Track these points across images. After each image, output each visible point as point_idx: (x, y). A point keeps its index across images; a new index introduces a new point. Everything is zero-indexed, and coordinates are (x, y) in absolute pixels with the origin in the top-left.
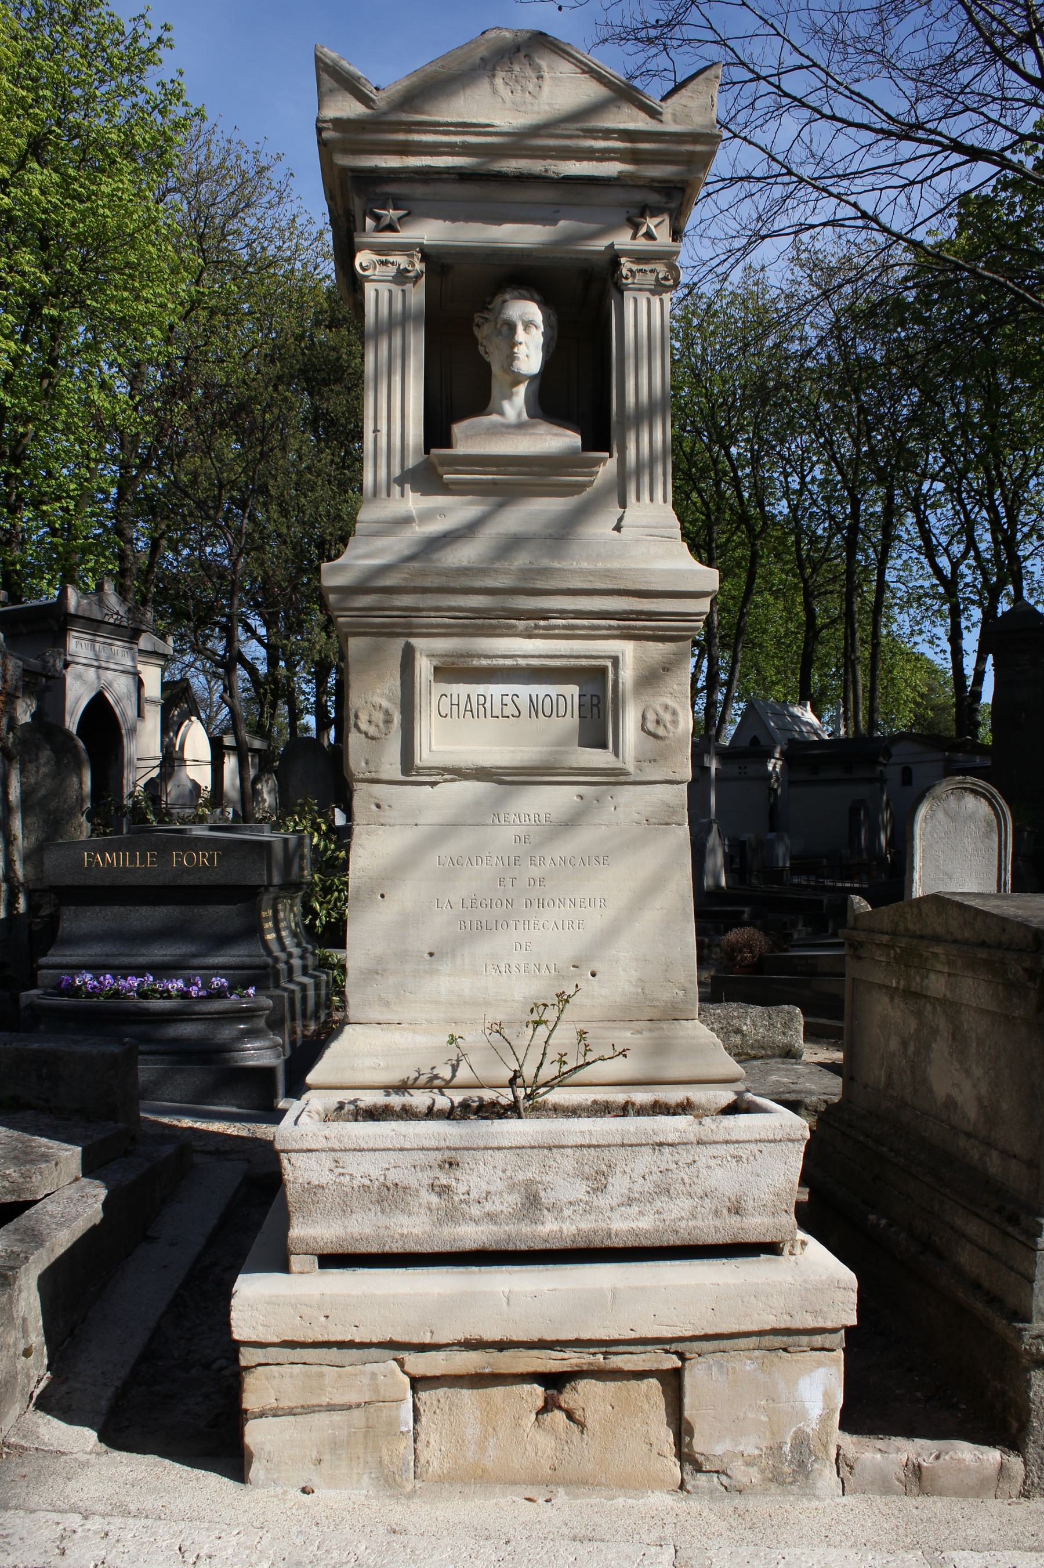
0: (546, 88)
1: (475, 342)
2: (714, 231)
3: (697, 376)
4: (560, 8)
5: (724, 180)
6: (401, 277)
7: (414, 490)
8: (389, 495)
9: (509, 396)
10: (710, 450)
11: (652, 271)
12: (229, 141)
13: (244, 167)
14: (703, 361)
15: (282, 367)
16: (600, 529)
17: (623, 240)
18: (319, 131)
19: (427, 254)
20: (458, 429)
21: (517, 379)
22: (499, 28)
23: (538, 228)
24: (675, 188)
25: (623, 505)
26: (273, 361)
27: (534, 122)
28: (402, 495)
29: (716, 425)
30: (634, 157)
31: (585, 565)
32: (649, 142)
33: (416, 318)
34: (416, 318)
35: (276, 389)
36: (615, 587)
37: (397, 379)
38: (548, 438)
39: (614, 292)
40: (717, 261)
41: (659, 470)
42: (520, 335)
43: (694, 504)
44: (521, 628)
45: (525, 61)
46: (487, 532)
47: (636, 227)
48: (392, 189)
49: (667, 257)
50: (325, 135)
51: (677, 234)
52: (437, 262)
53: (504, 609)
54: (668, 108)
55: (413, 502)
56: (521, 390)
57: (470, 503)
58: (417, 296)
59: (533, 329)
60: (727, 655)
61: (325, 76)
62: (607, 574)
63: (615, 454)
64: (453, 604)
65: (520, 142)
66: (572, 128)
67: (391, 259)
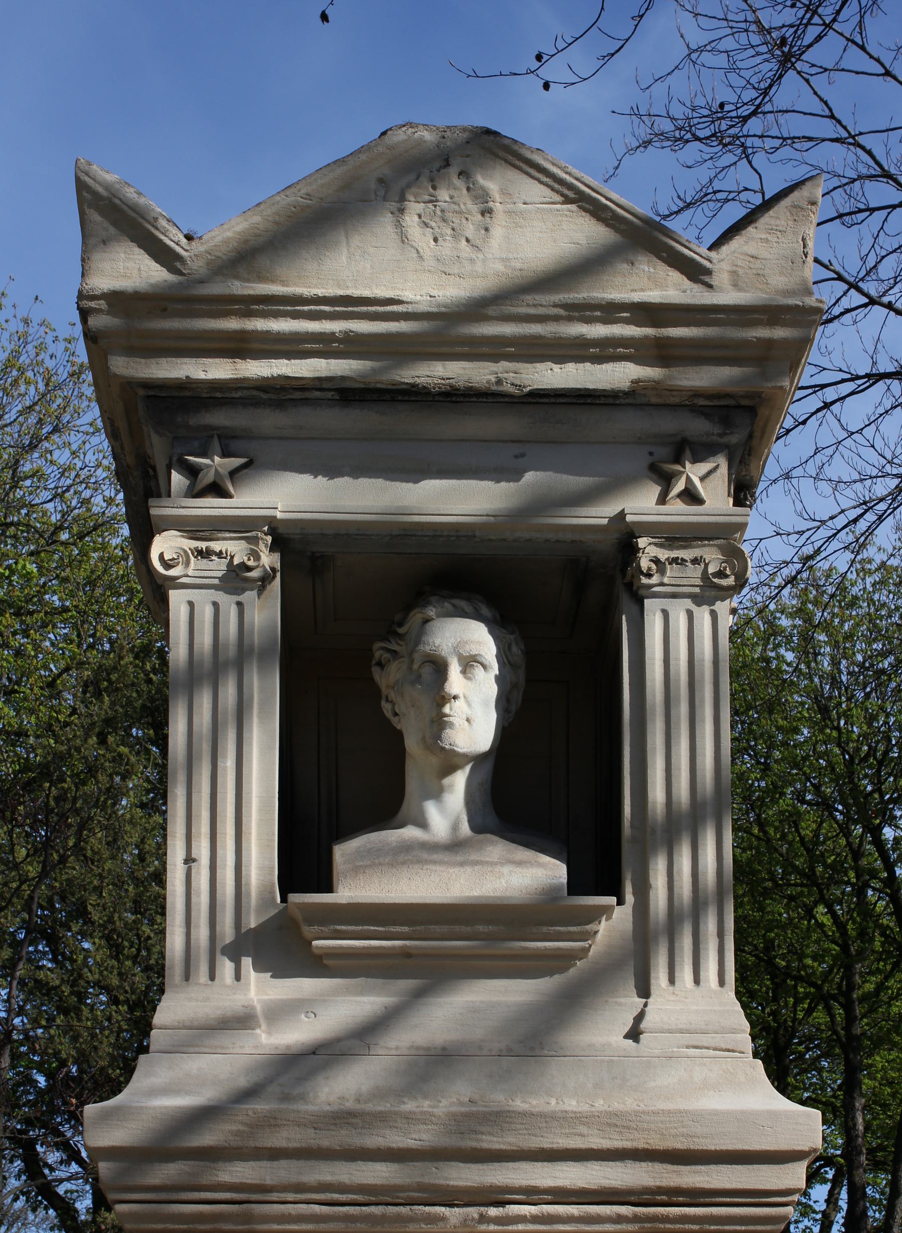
0: (497, 232)
1: (375, 694)
2: (839, 469)
3: (824, 710)
4: (546, 86)
5: (858, 377)
6: (236, 578)
8: (212, 977)
9: (437, 794)
10: (847, 834)
11: (695, 561)
12: (26, 322)
13: (50, 364)
14: (835, 682)
15: (113, 704)
16: (603, 1029)
17: (642, 503)
18: (84, 314)
19: (285, 537)
20: (342, 852)
21: (450, 762)
22: (410, 125)
23: (487, 485)
24: (738, 407)
25: (644, 991)
26: (98, 695)
27: (476, 293)
28: (238, 977)
29: (856, 789)
30: (661, 353)
31: (571, 1104)
32: (688, 325)
34: (264, 655)
35: (102, 741)
36: (628, 1145)
37: (228, 764)
38: (506, 870)
39: (625, 600)
40: (841, 521)
42: (455, 682)
43: (821, 926)
44: (454, 1221)
45: (457, 182)
46: (392, 1043)
47: (666, 480)
48: (219, 418)
49: (725, 535)
50: (92, 321)
51: (743, 492)
52: (301, 548)
53: (421, 1187)
54: (722, 262)
55: (258, 988)
56: (459, 781)
58: (265, 613)
59: (479, 671)
60: (883, 1179)
61: (95, 216)
62: (614, 1121)
63: (629, 898)
64: (328, 1178)
65: (447, 329)
66: (547, 300)
67: (216, 546)
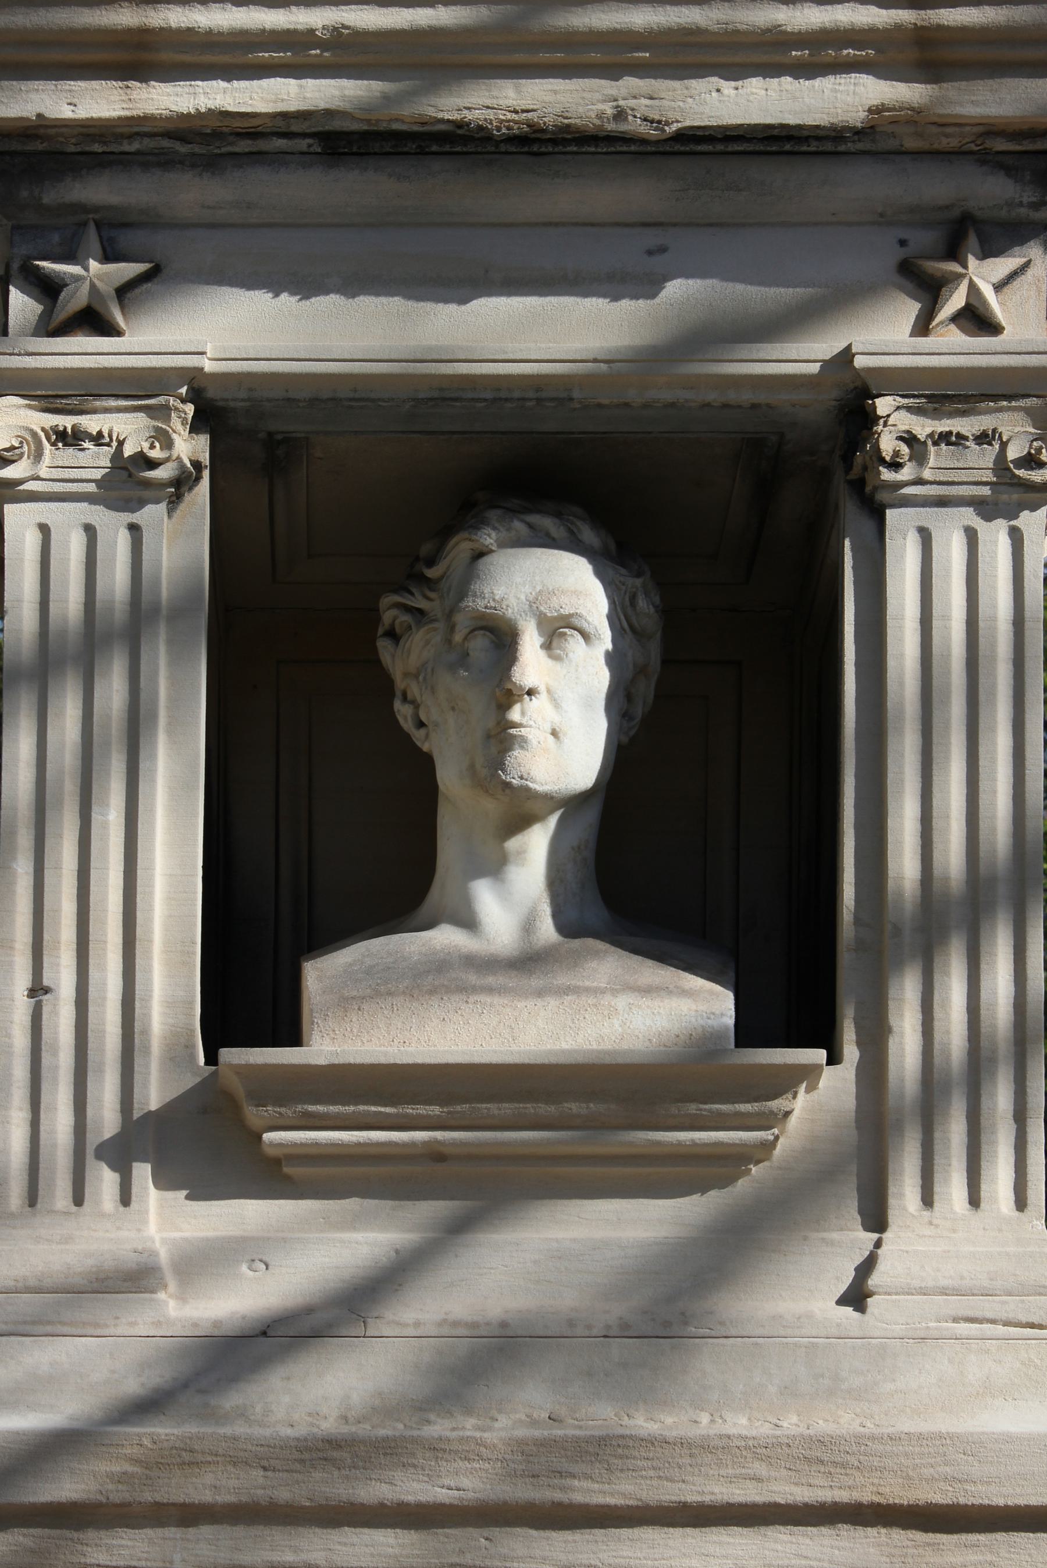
1: (383, 688)
6: (128, 482)
7: (163, 1181)
8: (78, 1200)
9: (495, 866)
11: (983, 438)
16: (798, 1292)
17: (884, 334)
19: (221, 408)
20: (319, 975)
21: (520, 810)
25: (876, 1219)
28: (125, 1199)
31: (738, 1424)
33: (178, 613)
36: (843, 1496)
37: (111, 817)
38: (621, 1002)
39: (850, 512)
41: (1001, 1098)
42: (532, 664)
47: (930, 291)
48: (98, 191)
52: (250, 431)
55: (162, 1219)
56: (536, 844)
57: (353, 1223)
58: (180, 542)
62: (817, 1453)
63: (851, 1052)
67: (91, 423)
